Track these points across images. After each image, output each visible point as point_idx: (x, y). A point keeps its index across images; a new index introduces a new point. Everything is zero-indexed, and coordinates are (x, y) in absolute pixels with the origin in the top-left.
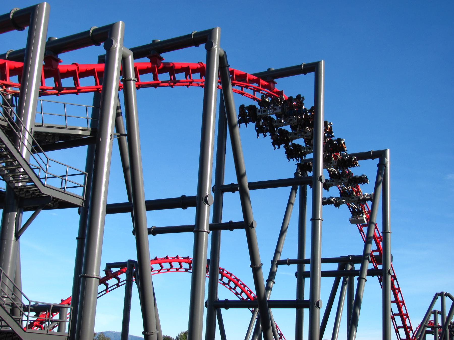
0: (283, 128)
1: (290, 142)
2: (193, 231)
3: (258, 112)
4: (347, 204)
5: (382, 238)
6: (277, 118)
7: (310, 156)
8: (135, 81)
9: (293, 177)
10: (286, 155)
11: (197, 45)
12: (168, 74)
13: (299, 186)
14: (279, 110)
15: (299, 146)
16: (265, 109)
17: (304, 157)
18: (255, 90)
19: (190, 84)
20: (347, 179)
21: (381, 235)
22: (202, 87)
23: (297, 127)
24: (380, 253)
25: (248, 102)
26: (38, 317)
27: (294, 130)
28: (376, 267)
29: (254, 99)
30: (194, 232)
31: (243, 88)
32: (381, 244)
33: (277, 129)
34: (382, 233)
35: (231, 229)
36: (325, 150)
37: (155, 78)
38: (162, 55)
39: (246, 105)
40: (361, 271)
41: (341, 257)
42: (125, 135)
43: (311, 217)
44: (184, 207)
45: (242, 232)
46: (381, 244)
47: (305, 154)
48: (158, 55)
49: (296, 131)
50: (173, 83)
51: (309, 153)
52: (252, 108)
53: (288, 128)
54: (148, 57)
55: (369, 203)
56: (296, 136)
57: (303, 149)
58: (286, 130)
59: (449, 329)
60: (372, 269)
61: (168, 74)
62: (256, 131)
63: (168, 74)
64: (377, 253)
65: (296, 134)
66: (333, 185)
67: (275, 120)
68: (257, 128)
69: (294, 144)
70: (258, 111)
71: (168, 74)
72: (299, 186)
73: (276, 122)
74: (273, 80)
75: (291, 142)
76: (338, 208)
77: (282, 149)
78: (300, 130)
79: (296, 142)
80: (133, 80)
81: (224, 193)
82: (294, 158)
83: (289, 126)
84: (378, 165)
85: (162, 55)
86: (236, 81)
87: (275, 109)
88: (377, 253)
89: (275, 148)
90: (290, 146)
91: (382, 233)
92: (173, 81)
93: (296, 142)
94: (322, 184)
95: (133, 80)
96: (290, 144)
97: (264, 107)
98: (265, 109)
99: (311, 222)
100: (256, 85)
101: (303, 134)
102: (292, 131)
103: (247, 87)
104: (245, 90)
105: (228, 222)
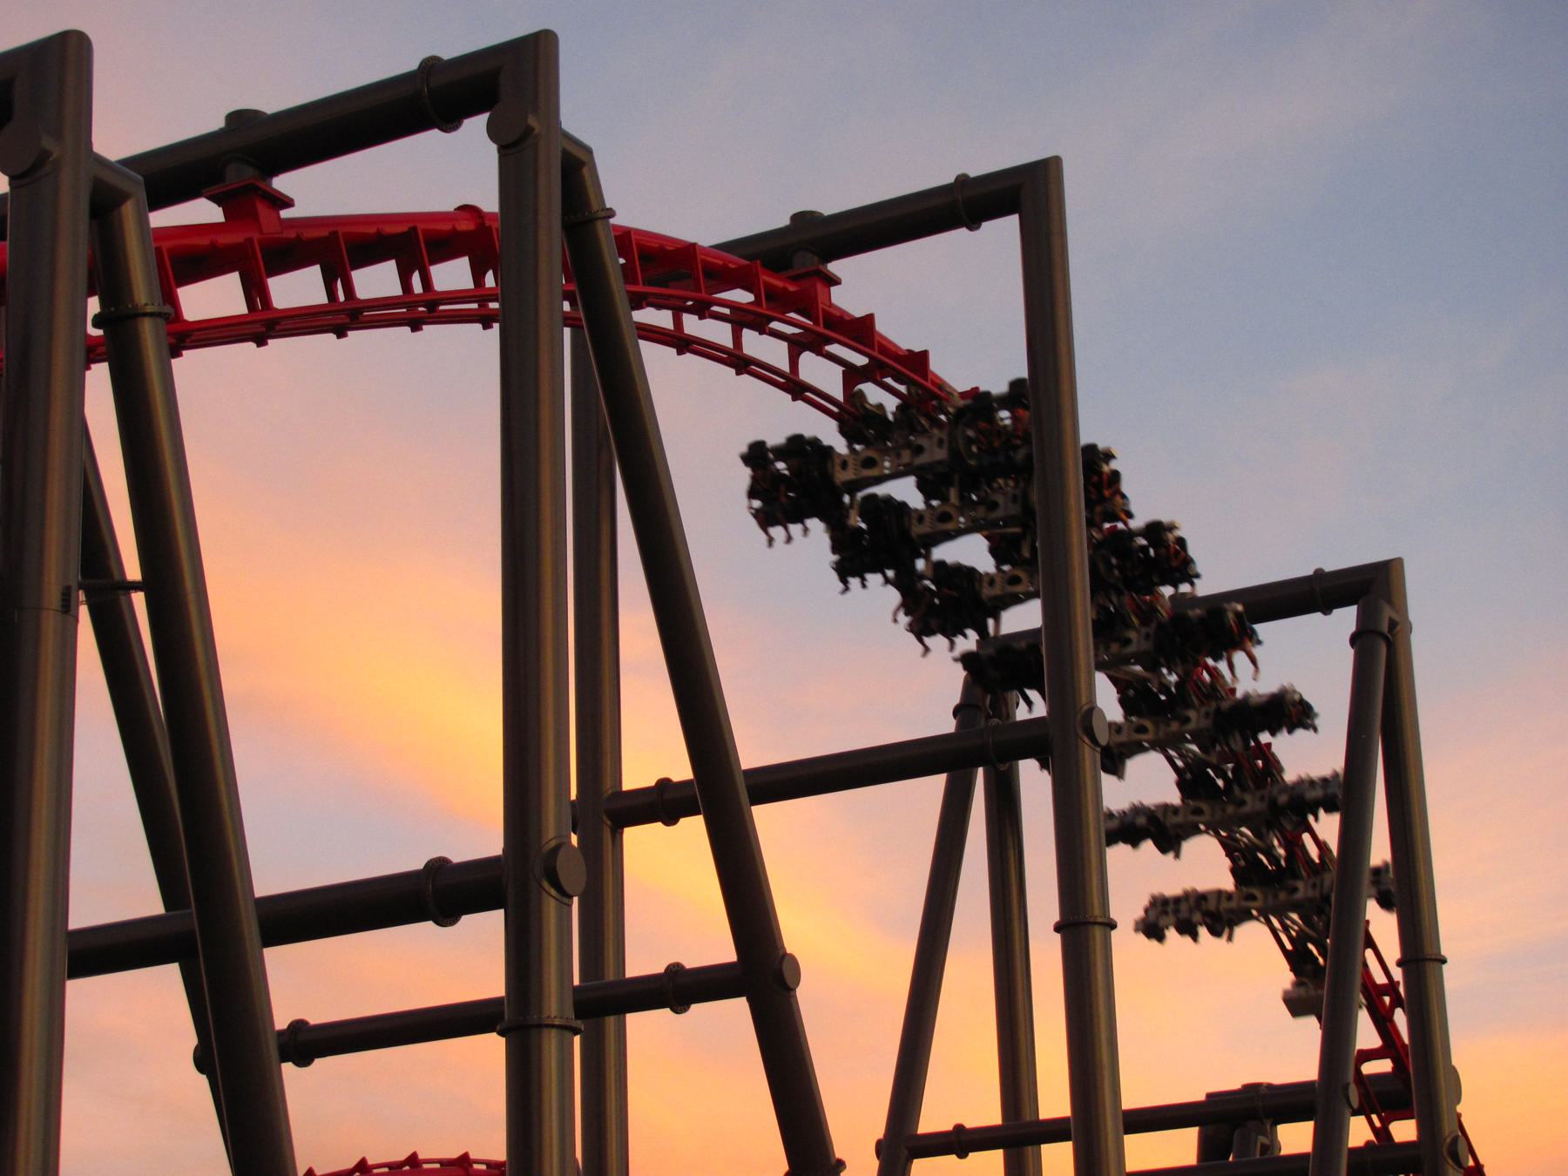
0: (881, 490)
1: (919, 556)
2: (498, 1028)
3: (838, 468)
4: (1217, 835)
5: (1401, 989)
6: (850, 446)
7: (1023, 618)
8: (161, 321)
9: (948, 725)
10: (835, 558)
11: (449, 122)
13: (980, 771)
14: (936, 453)
15: (963, 575)
16: (871, 453)
17: (991, 622)
18: (741, 319)
20: (1207, 714)
21: (1397, 974)
22: (487, 326)
24: (1399, 1065)
26: (74, 587)
27: (935, 499)
28: (1382, 1134)
29: (796, 388)
30: (503, 1036)
32: (1400, 1018)
34: (1399, 963)
35: (680, 1005)
36: (1099, 584)
37: (255, 291)
38: (283, 183)
39: (775, 439)
41: (1209, 1096)
42: (135, 586)
43: (1055, 916)
44: (446, 916)
45: (735, 1013)
46: (1400, 1018)
47: (995, 611)
48: (261, 184)
49: (944, 499)
51: (1016, 600)
52: (799, 448)
53: (905, 491)
54: (212, 198)
55: (1328, 826)
56: (949, 526)
57: (985, 584)
59: (1429, 1127)
60: (1368, 1143)
64: (1384, 1066)
66: (1140, 749)
67: (840, 454)
68: (757, 504)
69: (941, 565)
70: (838, 461)
72: (980, 771)
73: (844, 465)
75: (927, 557)
76: (1177, 856)
77: (814, 539)
78: (963, 497)
79: (947, 552)
80: (152, 315)
81: (625, 829)
82: (1030, 688)
84: (1354, 640)
85: (283, 183)
86: (644, 284)
87: (919, 450)
88: (1384, 1066)
89: (847, 589)
90: (922, 577)
91: (1399, 963)
92: (343, 307)
93: (947, 552)
95: (152, 315)
96: (920, 564)
98: (871, 453)
99: (1058, 936)
100: (742, 296)
101: (981, 512)
102: (927, 502)
103: (702, 311)
104: (693, 325)
105: (663, 971)
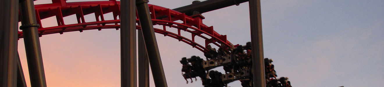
0: (215, 70)
6: (207, 59)
8: (36, 28)
12: (74, 16)
14: (228, 60)
18: (180, 27)
19: (100, 25)
22: (117, 29)
23: (232, 68)
25: (190, 52)
29: (194, 44)
31: (166, 26)
33: (208, 72)
37: (60, 20)
39: (189, 57)
40: (82, 15)
49: (230, 72)
50: (82, 27)
52: (195, 59)
53: (221, 70)
56: (232, 78)
58: (219, 71)
61: (74, 16)
62: (183, 76)
63: (75, 16)
65: (231, 76)
68: (184, 73)
70: (204, 62)
71: (75, 16)
73: (206, 63)
74: (200, 15)
80: (34, 26)
83: (222, 67)
94: (183, 75)
95: (34, 26)
97: (211, 58)
98: (212, 60)
100: (180, 22)
101: (239, 75)
103: (171, 25)
104: (168, 29)
